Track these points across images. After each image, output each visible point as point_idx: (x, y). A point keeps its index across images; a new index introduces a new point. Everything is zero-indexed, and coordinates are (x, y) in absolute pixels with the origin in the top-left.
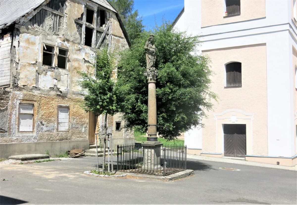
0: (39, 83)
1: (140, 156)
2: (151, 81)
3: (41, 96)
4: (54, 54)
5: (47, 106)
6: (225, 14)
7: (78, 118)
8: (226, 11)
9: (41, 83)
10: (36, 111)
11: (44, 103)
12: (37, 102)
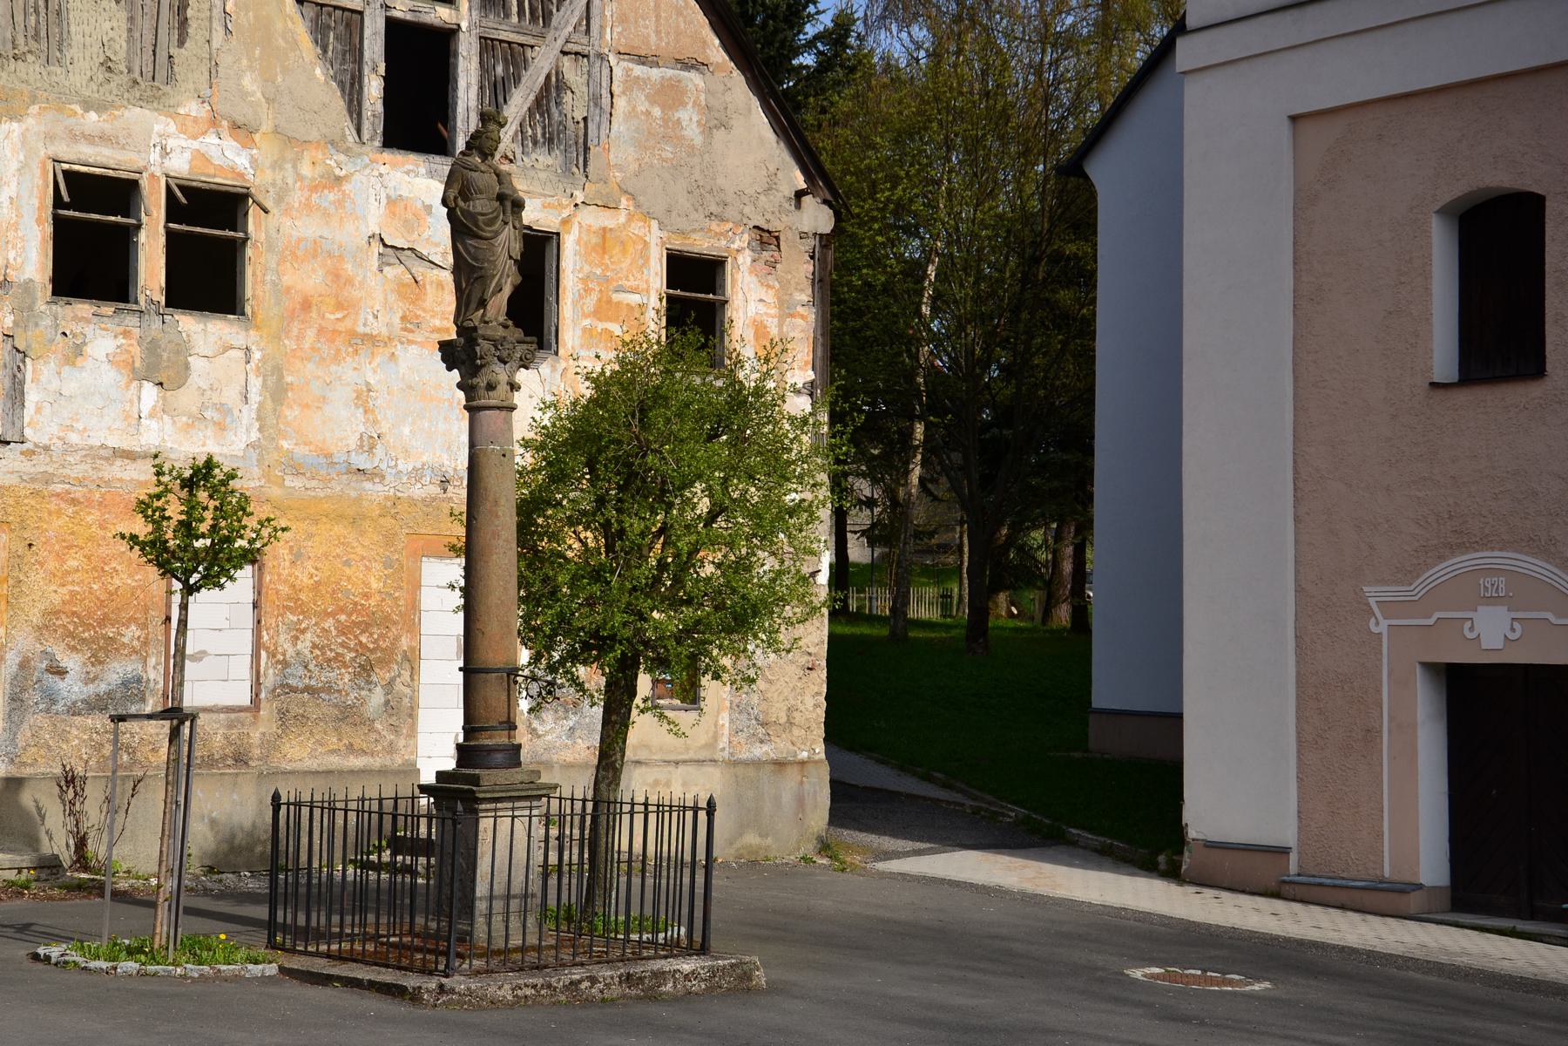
5: (86, 551)
7: (329, 623)
9: (38, 410)
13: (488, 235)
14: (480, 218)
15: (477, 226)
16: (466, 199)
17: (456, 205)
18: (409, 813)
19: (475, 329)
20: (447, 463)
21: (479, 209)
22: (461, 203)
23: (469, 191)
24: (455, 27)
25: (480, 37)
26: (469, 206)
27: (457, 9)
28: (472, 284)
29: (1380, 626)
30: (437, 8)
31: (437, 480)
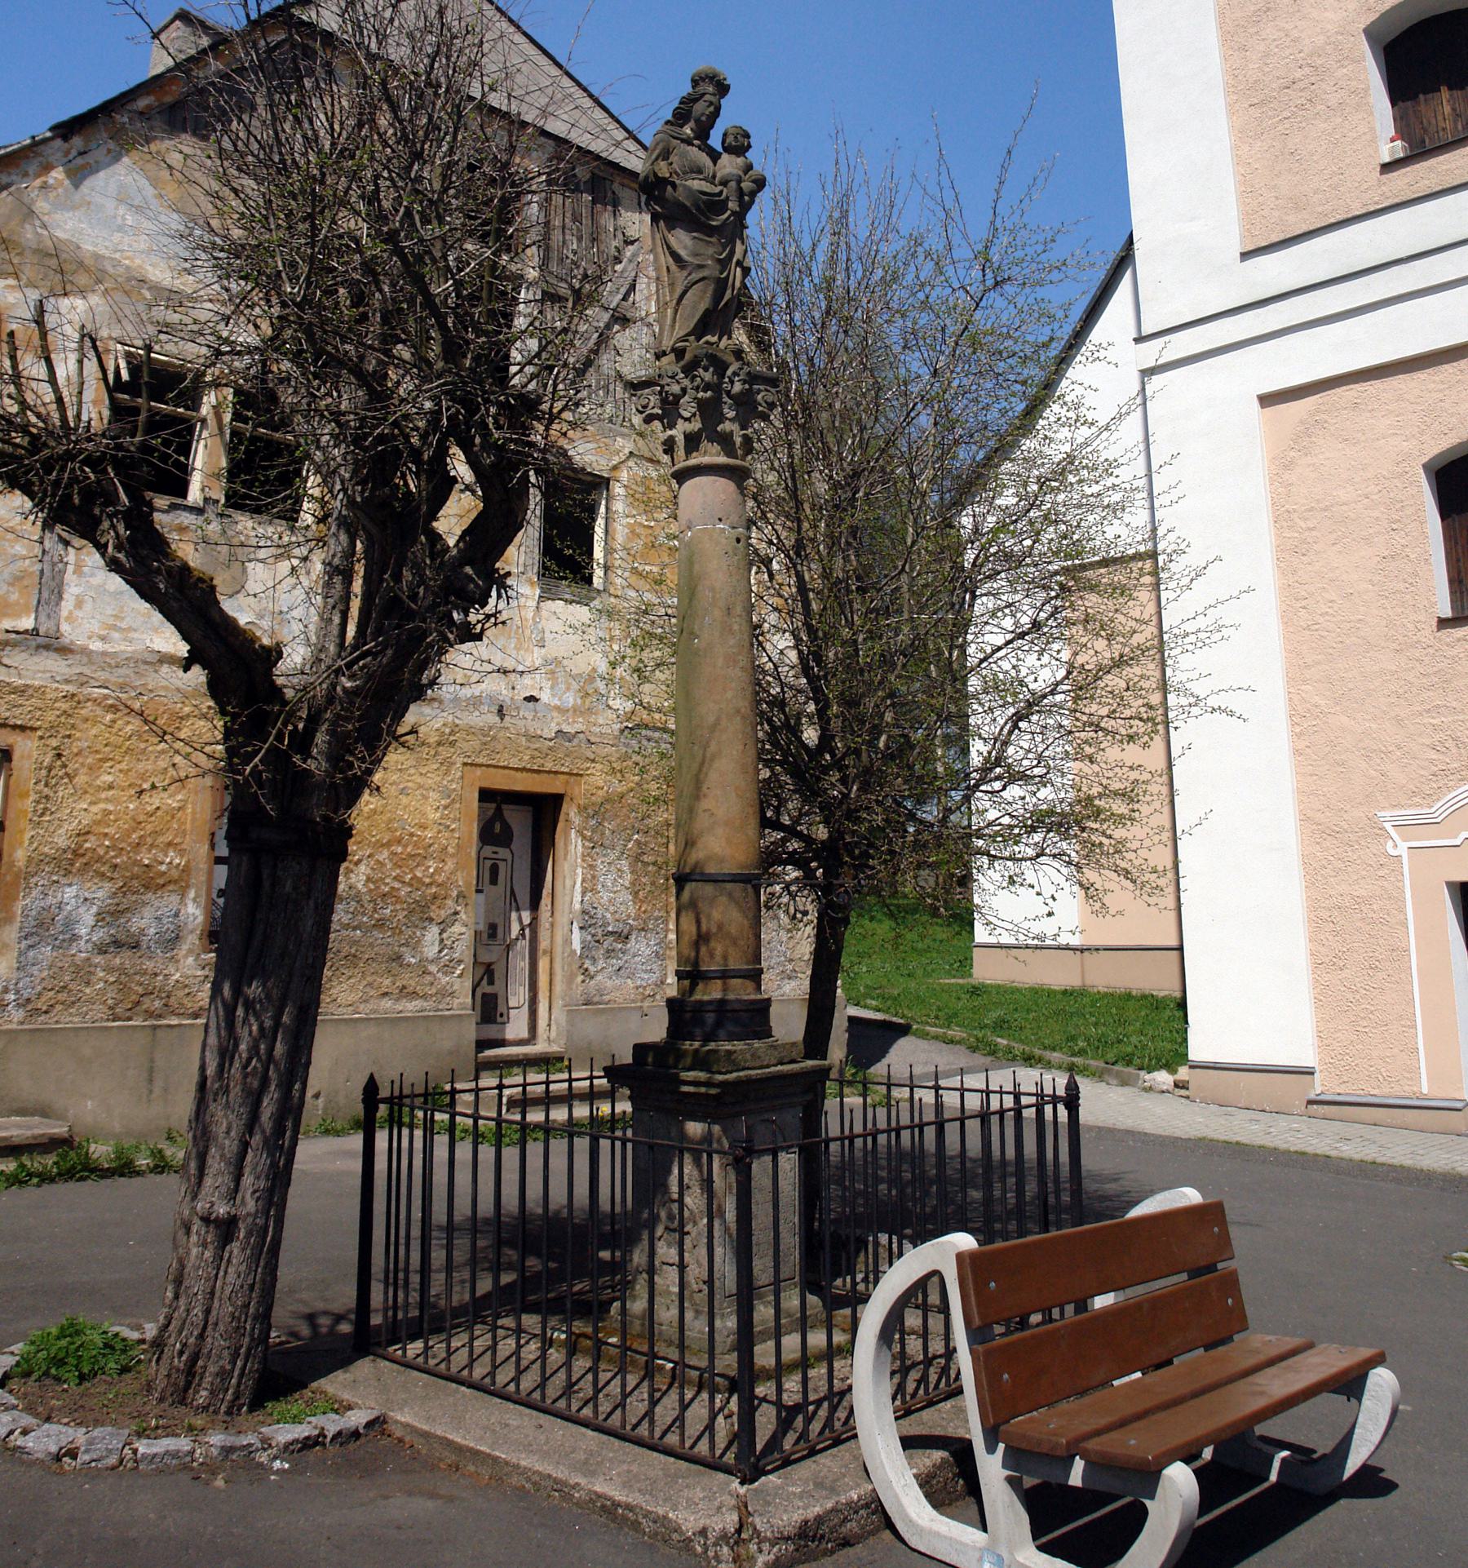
0: (67, 605)
1: (558, 1196)
2: (692, 462)
3: (73, 695)
4: (204, 421)
5: (123, 766)
6: (1389, 148)
7: (384, 855)
8: (1392, 133)
9: (79, 604)
10: (29, 803)
11: (99, 747)
12: (41, 738)
20: (504, 692)
29: (1400, 847)
31: (495, 709)
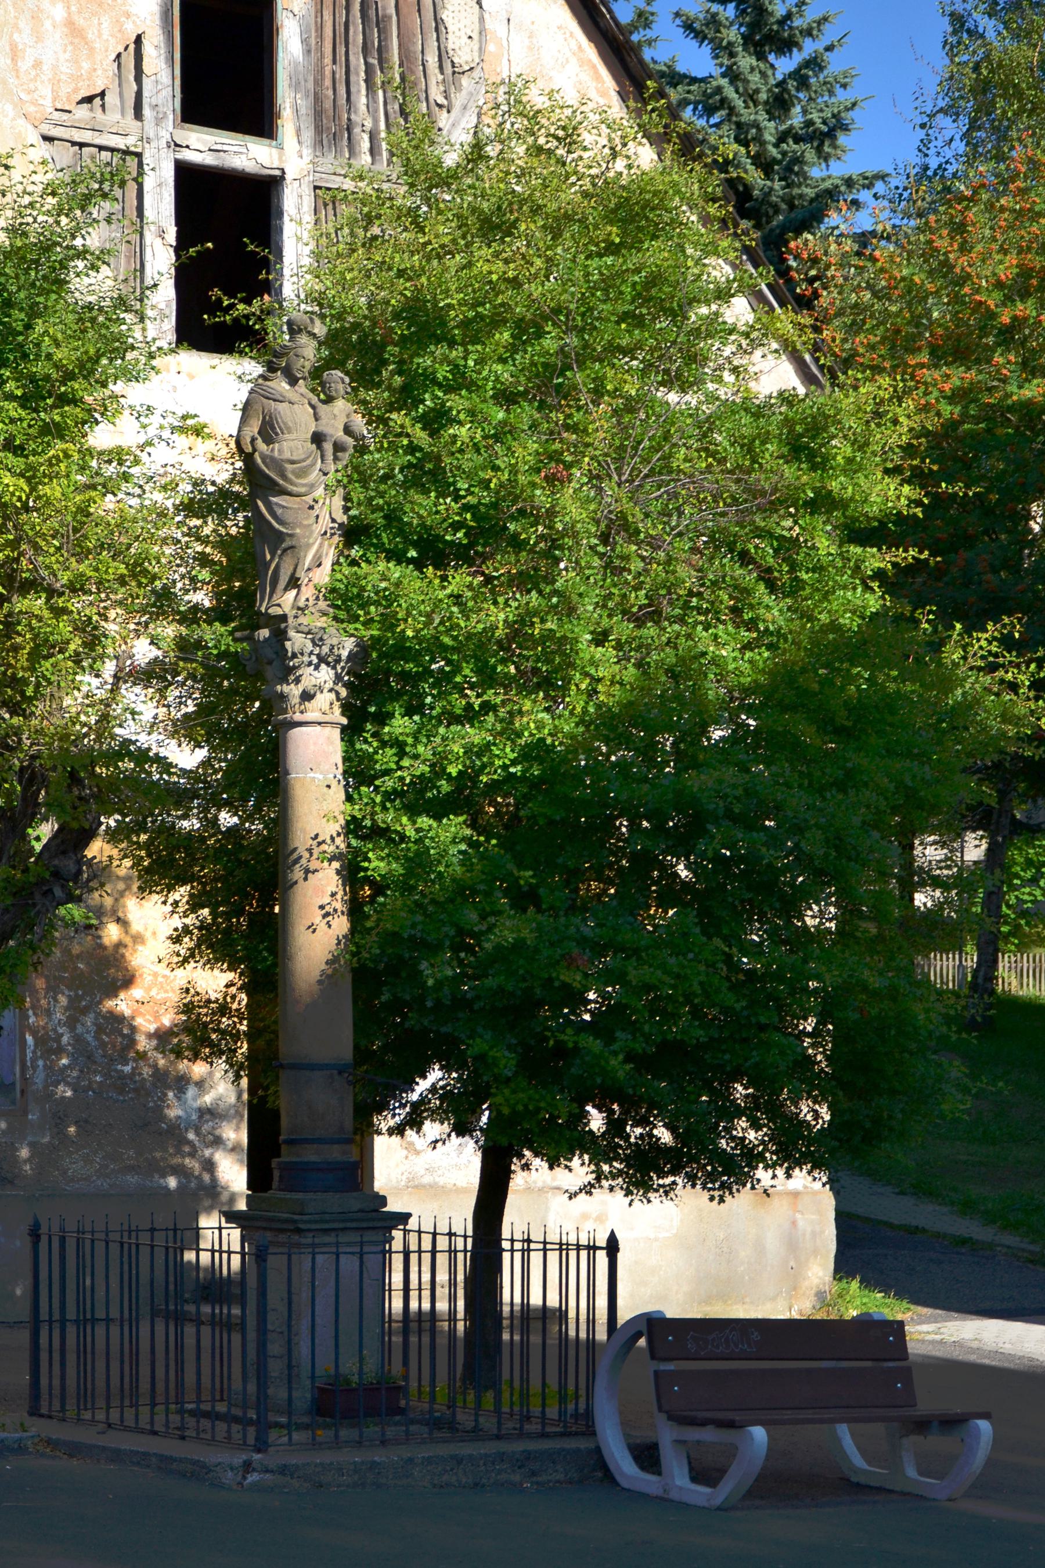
13: (303, 490)
14: (289, 467)
15: (284, 477)
16: (268, 440)
17: (255, 450)
18: (217, 1247)
19: (284, 618)
21: (287, 455)
22: (261, 445)
23: (273, 428)
24: (278, 173)
25: (316, 188)
26: (273, 450)
27: (280, 147)
28: (280, 557)
30: (249, 145)
